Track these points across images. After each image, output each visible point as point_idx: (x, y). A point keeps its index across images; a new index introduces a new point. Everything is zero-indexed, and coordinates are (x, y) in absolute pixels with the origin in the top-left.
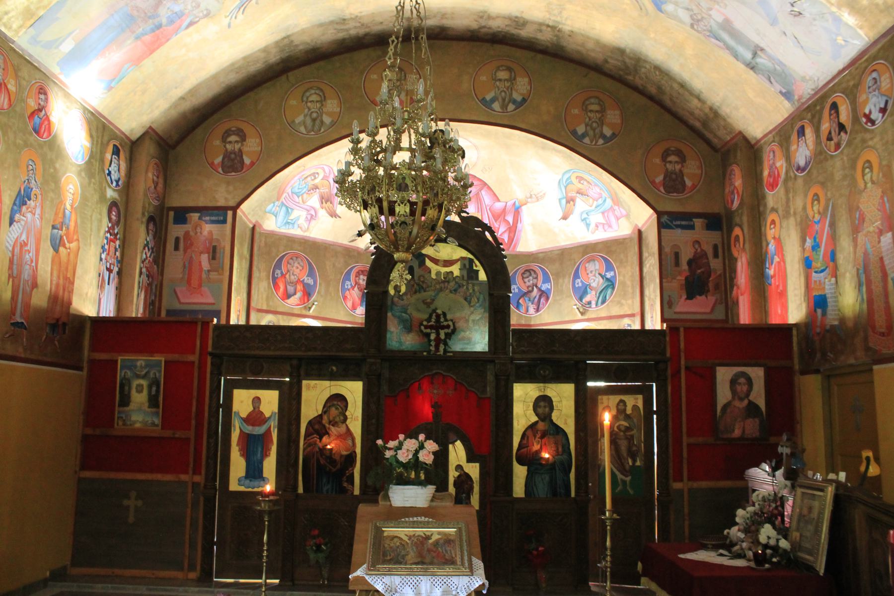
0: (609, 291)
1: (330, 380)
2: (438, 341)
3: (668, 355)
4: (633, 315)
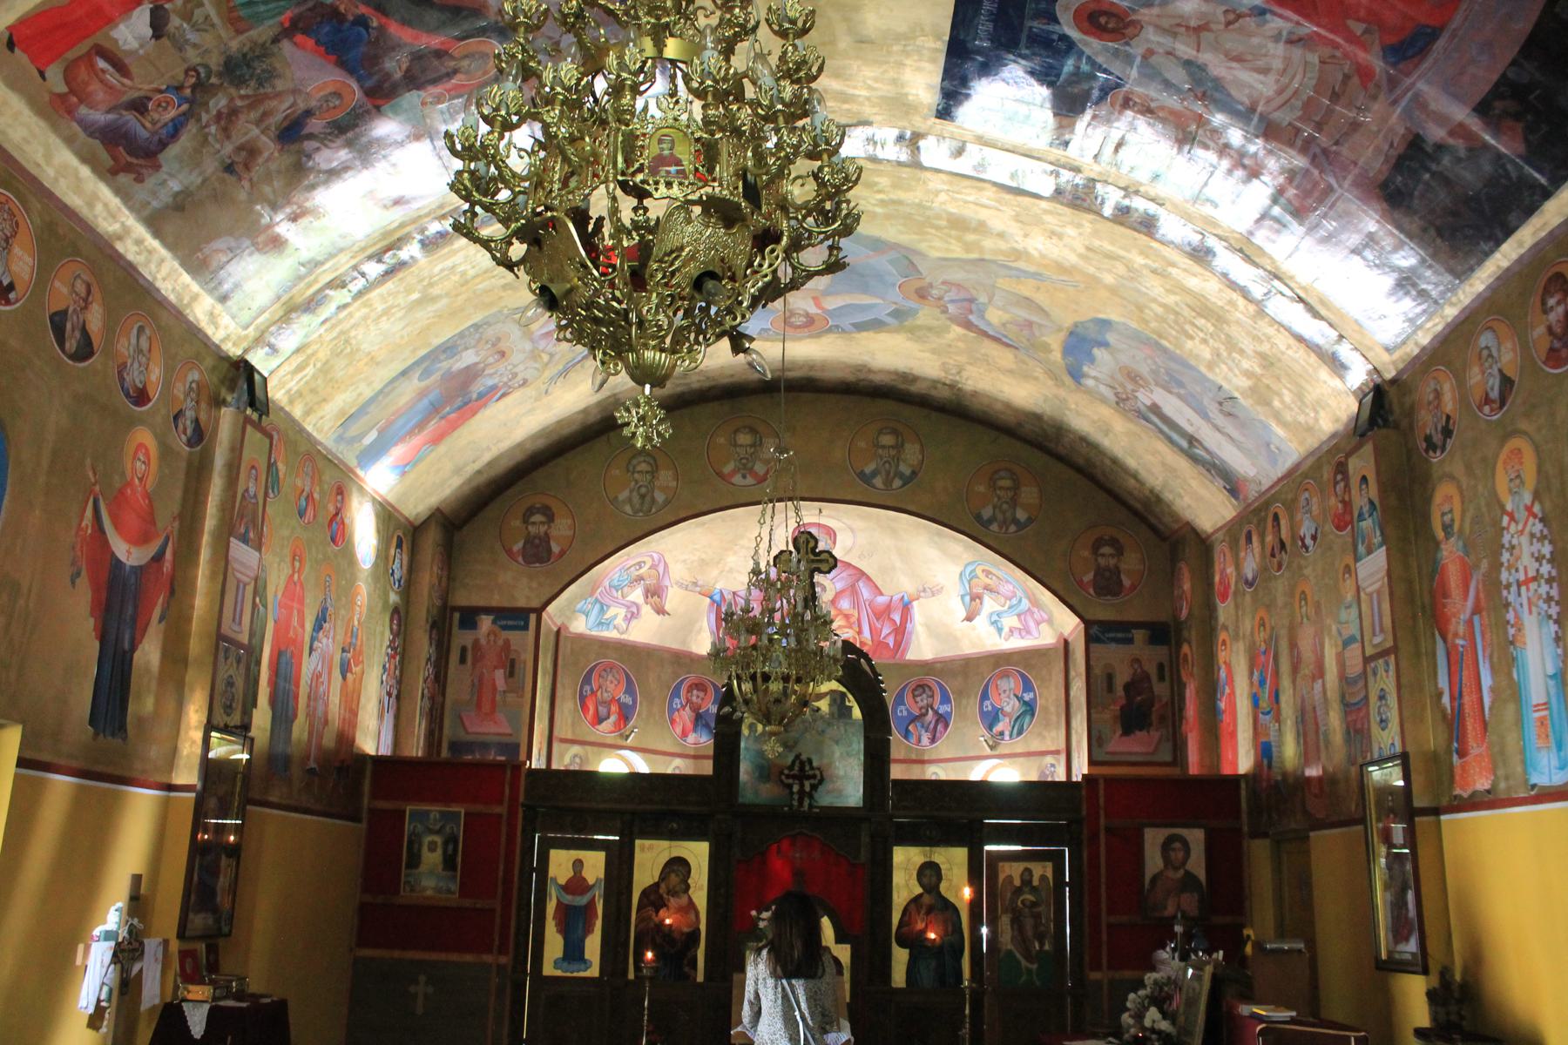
0: (1027, 719)
1: (671, 839)
2: (802, 792)
3: (1084, 813)
4: (1057, 752)
